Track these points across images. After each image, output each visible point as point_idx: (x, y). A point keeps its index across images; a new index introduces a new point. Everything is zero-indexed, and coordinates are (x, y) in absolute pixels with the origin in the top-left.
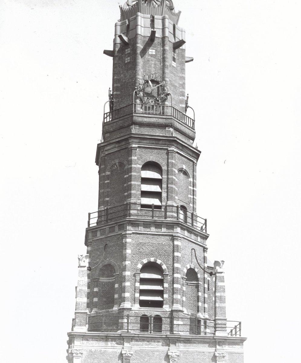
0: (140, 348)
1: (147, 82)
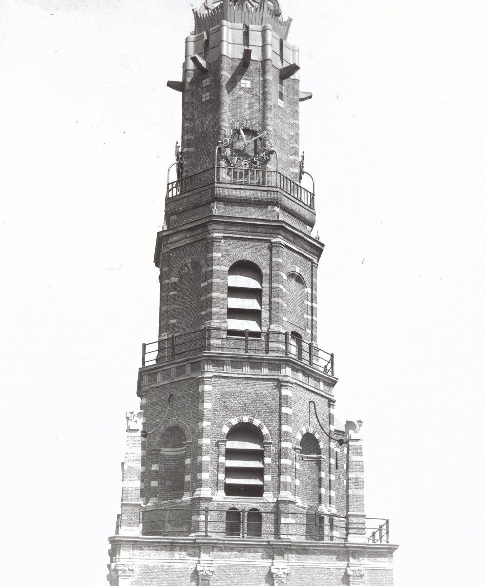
0: (227, 562)
1: (238, 132)
